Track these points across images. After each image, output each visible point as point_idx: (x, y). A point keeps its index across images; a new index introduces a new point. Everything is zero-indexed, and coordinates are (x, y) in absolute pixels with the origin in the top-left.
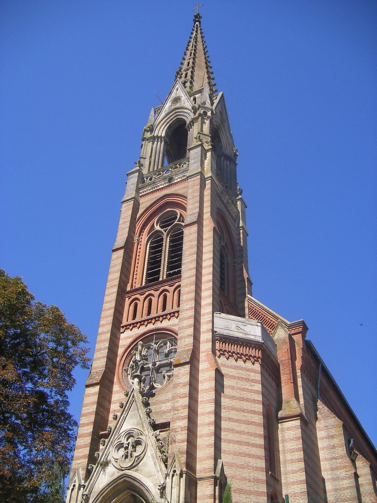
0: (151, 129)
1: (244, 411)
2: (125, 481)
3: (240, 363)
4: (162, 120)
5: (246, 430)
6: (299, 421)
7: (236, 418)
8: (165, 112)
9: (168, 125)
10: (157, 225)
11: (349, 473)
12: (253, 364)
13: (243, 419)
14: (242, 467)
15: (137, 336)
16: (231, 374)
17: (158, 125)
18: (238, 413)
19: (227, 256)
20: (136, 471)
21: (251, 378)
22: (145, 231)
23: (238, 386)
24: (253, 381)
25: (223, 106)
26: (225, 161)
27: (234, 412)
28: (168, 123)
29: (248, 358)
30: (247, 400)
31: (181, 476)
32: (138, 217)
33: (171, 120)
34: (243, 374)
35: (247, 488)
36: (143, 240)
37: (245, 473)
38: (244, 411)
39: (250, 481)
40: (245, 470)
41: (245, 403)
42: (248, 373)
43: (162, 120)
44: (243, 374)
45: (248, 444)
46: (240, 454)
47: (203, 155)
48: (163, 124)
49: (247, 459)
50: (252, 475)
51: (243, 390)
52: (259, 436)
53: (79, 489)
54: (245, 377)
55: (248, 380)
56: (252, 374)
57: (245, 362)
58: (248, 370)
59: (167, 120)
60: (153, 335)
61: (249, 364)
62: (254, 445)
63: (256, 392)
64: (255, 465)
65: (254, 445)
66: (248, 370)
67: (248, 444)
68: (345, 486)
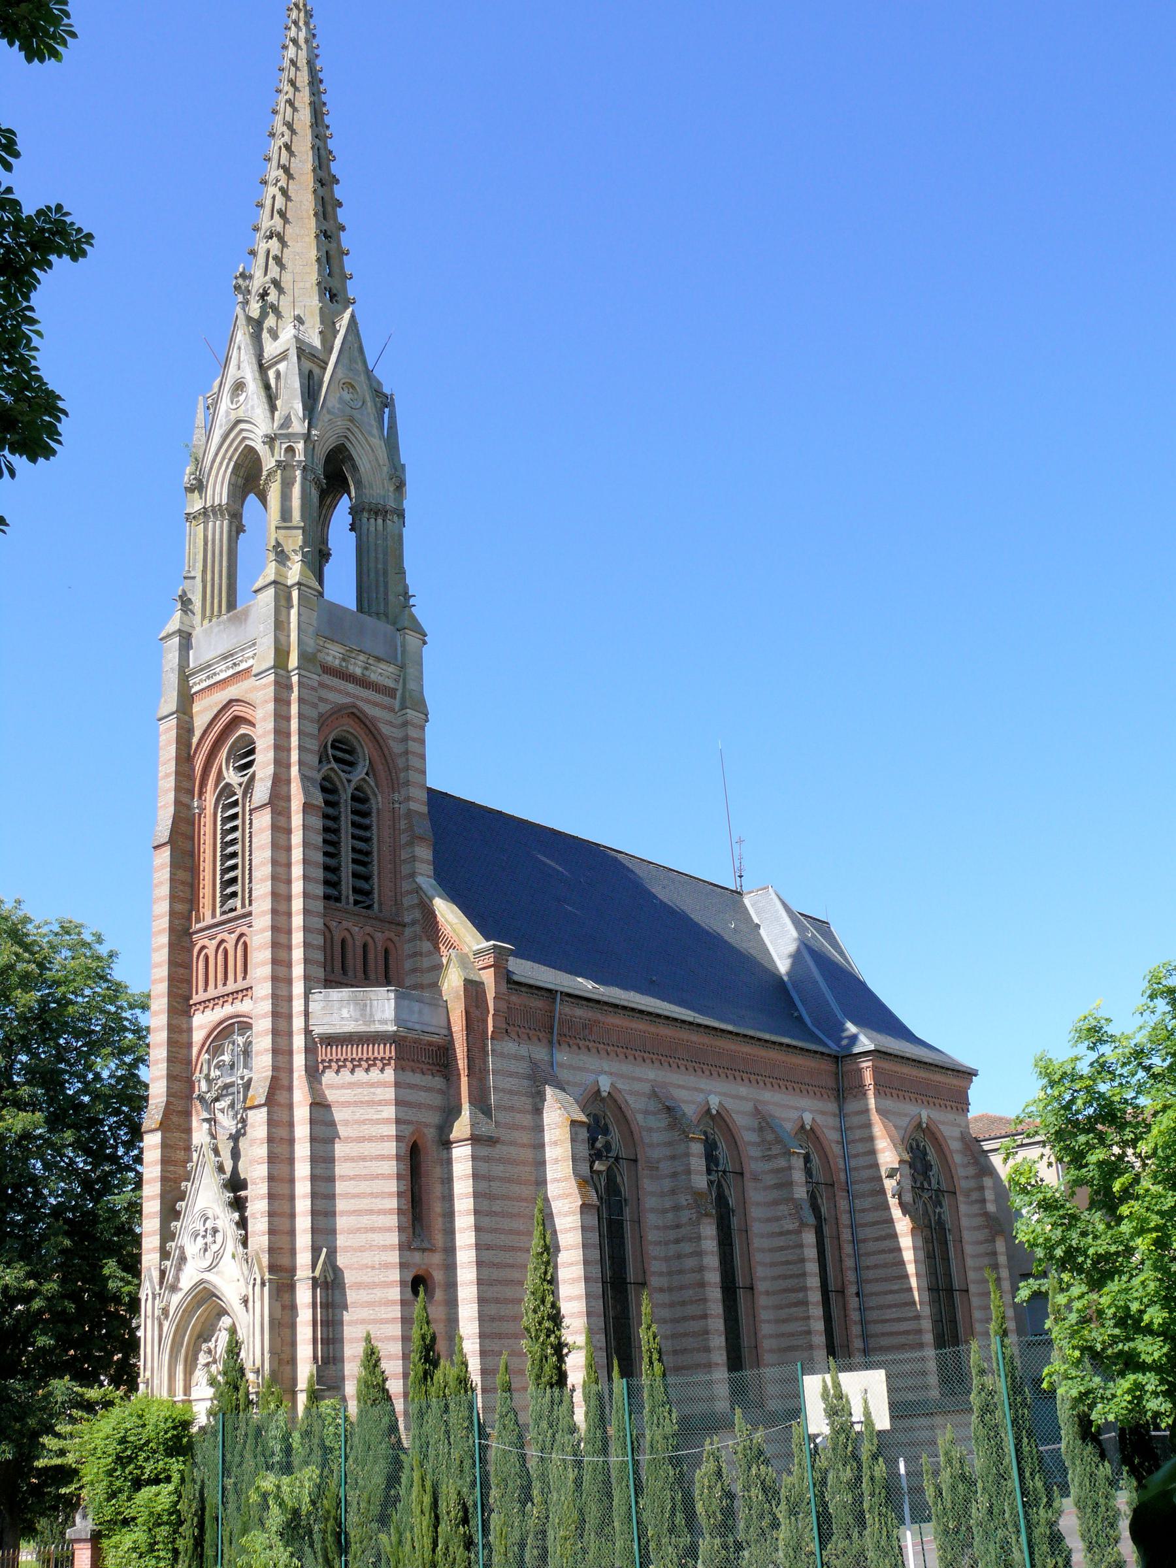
0: (199, 486)
1: (363, 1159)
2: (205, 1288)
3: (360, 1074)
4: (217, 454)
5: (369, 1190)
6: (469, 1147)
7: (352, 1173)
8: (221, 426)
9: (232, 464)
10: (228, 769)
11: (573, 1205)
12: (382, 1070)
13: (365, 1172)
14: (361, 1249)
15: (212, 1025)
16: (342, 1099)
17: (211, 468)
18: (354, 1165)
19: (375, 795)
20: (217, 1273)
21: (377, 1098)
22: (209, 787)
23: (356, 1117)
24: (380, 1103)
25: (356, 354)
26: (372, 520)
27: (348, 1164)
28: (230, 459)
29: (371, 1064)
30: (370, 1139)
31: (263, 1284)
32: (195, 740)
33: (236, 450)
34: (364, 1094)
35: (369, 1280)
36: (207, 803)
37: (367, 1258)
38: (363, 1159)
39: (373, 1268)
40: (366, 1254)
41: (367, 1145)
42: (372, 1090)
43: (217, 454)
44: (364, 1094)
45: (371, 1212)
46: (358, 1230)
47: (283, 603)
48: (221, 463)
49: (370, 1236)
50: (376, 1259)
51: (364, 1122)
52: (390, 1195)
53: (154, 1298)
54: (366, 1098)
55: (371, 1103)
56: (379, 1091)
57: (367, 1070)
58: (372, 1085)
59: (227, 451)
60: (233, 1024)
61: (375, 1074)
62: (381, 1212)
63: (386, 1121)
64: (382, 1243)
65: (381, 1212)
66: (372, 1085)
67: (371, 1212)
68: (568, 1226)
